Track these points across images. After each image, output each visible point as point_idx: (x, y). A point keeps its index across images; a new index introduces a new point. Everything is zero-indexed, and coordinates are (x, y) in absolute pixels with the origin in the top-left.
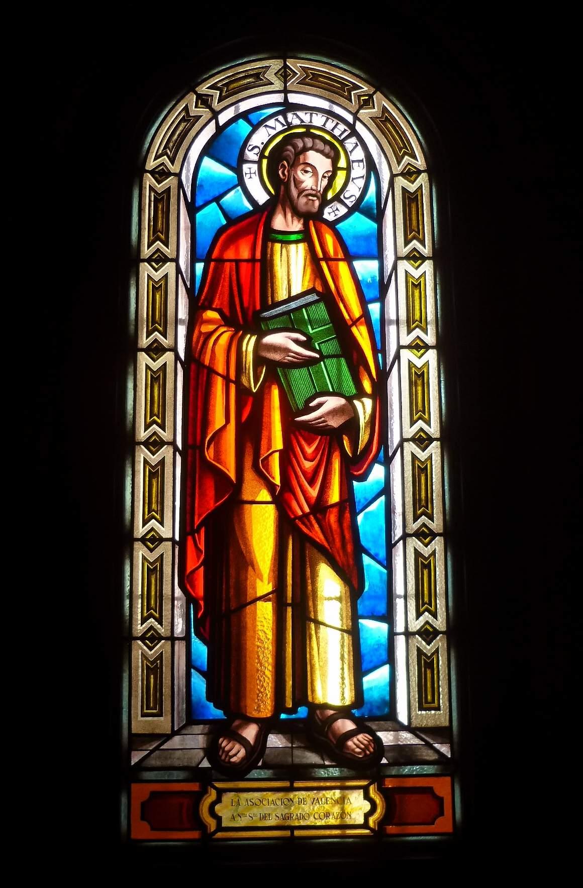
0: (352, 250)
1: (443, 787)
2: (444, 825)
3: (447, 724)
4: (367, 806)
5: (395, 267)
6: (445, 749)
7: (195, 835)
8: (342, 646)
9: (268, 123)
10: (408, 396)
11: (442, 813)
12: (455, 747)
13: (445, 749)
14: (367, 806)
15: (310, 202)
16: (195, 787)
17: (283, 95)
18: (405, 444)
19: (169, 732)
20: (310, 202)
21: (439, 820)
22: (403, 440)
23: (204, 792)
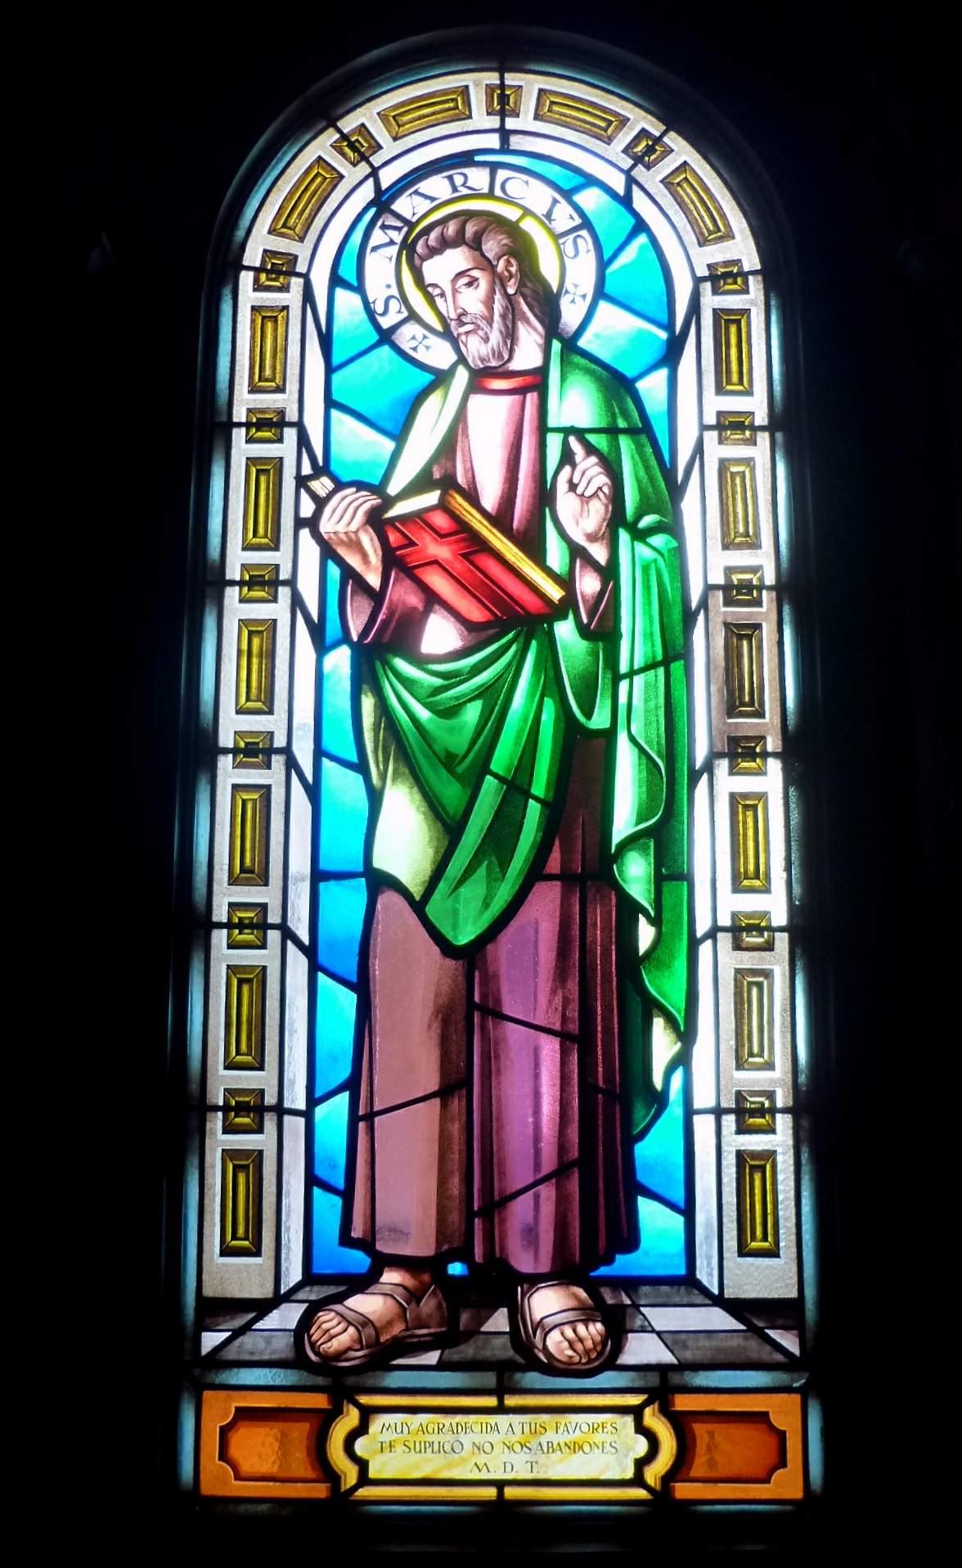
0: (609, 288)
1: (784, 1411)
2: (787, 1485)
3: (794, 1294)
4: (641, 1446)
5: (699, 449)
6: (790, 1342)
7: (320, 1491)
8: (612, 93)
9: (372, 243)
10: (718, 515)
11: (782, 1463)
12: (809, 1335)
13: (790, 1342)
14: (641, 1446)
15: (503, 344)
16: (320, 1401)
17: (287, 1118)
18: (720, 935)
19: (266, 1291)
20: (503, 344)
21: (777, 1421)
22: (709, 588)
23: (335, 1413)
